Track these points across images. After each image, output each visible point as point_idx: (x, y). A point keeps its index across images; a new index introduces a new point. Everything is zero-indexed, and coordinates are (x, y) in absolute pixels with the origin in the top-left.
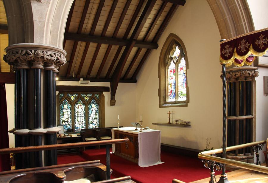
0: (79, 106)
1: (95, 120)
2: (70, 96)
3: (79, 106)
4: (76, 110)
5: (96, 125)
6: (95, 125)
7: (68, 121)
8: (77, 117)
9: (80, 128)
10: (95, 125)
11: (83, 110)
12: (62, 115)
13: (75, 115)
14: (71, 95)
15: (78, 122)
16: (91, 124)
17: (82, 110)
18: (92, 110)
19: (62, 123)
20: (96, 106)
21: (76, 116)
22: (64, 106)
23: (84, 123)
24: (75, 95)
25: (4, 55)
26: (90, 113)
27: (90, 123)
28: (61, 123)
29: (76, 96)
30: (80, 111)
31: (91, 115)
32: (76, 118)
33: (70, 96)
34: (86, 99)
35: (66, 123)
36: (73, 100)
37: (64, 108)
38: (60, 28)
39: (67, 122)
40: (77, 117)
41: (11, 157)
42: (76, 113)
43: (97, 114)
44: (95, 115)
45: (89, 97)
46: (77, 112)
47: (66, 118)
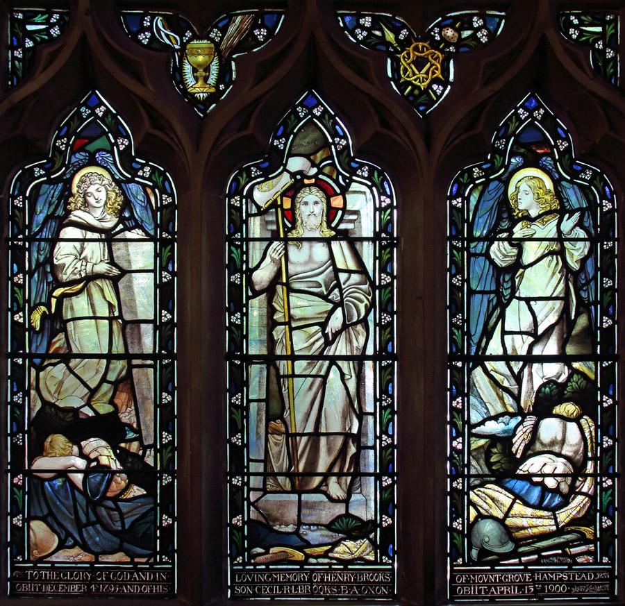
0: (293, 191)
1: (550, 429)
2: (167, 37)
3: (293, 191)
4: (256, 251)
5: (578, 504)
6: (549, 500)
7: (127, 417)
8: (270, 359)
9: (314, 536)
10: (549, 500)
11: (367, 251)
12: (36, 318)
13: (240, 335)
14: (174, 25)
15: (277, 445)
16: (492, 490)
17: (343, 255)
18: (500, 252)
19: (38, 450)
20: (574, 198)
21: (255, 347)
22: (66, 194)
23: (370, 460)
24: (238, 22)
25: (556, 437)
26: (479, 306)
27: (476, 467)
28: (24, 440)
29: (247, 41)
30: (275, 407)
31: (494, 347)
32: (256, 373)
33: (167, 37)
34: (418, 78)
35: (98, 448)
36: (199, 90)
37: (64, 222)
38: (378, 491)
39: (110, 428)
40: (270, 359)
41: (166, 361)
42: (256, 308)
43: (590, 330)
44: (551, 347)
45: (466, 53)
46: (262, 276)
47: (92, 372)
